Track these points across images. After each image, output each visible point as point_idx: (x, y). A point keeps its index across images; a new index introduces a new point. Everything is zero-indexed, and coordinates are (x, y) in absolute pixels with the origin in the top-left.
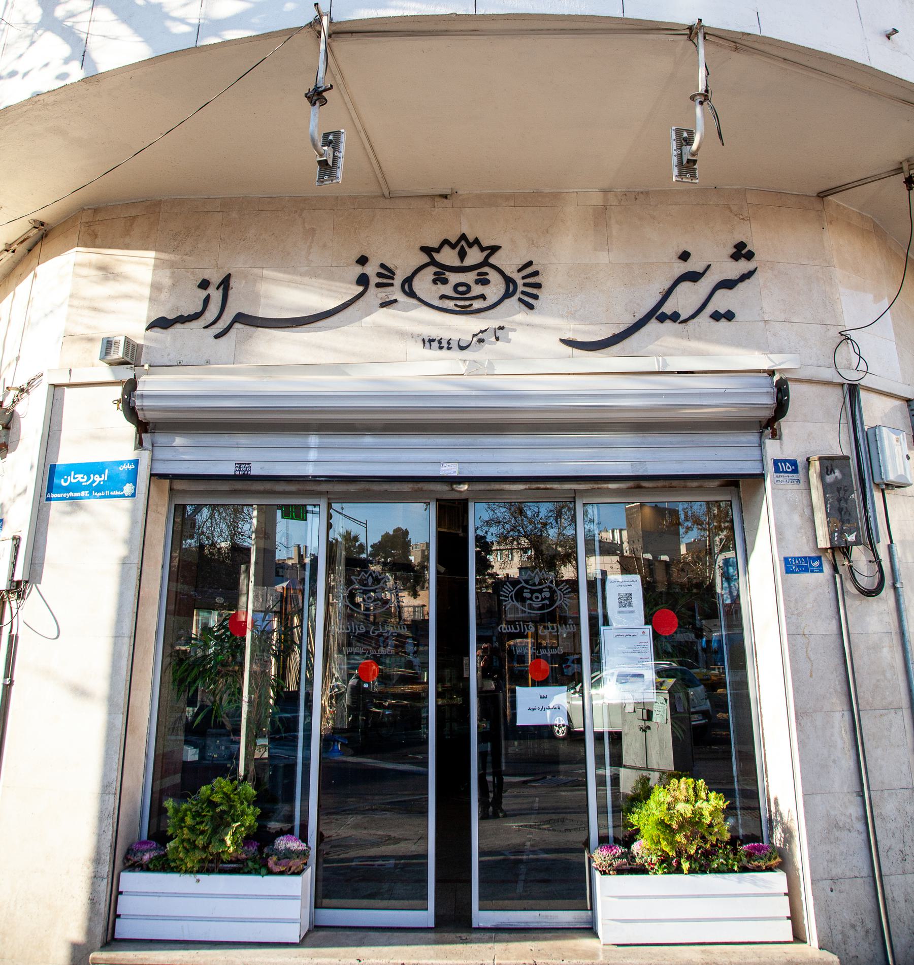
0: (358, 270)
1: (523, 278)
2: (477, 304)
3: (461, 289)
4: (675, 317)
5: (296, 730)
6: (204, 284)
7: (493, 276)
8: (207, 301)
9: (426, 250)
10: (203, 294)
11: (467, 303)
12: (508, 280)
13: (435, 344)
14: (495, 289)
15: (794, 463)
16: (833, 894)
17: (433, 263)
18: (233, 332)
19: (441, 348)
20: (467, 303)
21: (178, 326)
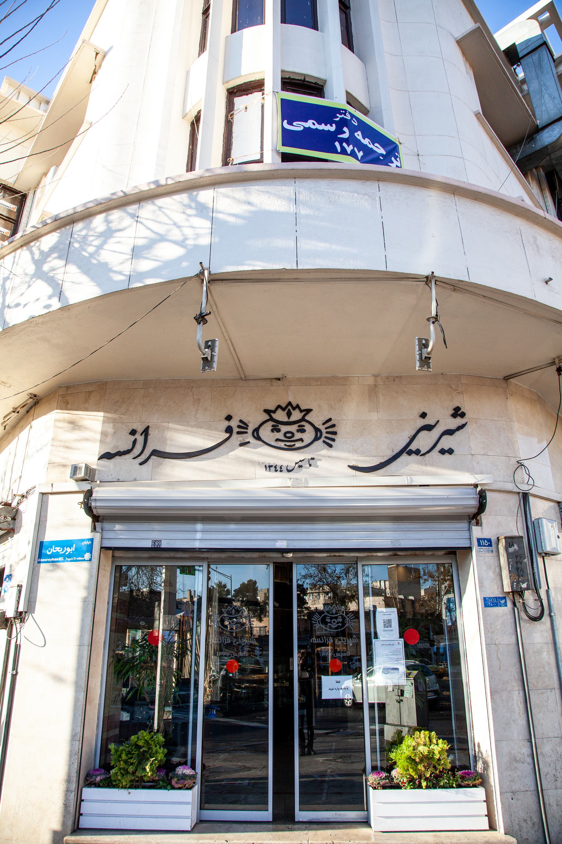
0: (226, 424)
1: (326, 428)
2: (298, 444)
3: (288, 435)
4: (417, 452)
7: (308, 427)
8: (135, 442)
9: (267, 411)
10: (132, 438)
11: (292, 444)
12: (317, 430)
13: (273, 469)
15: (489, 540)
16: (513, 801)
17: (272, 419)
18: (150, 461)
19: (276, 471)
20: (292, 444)
21: (117, 457)
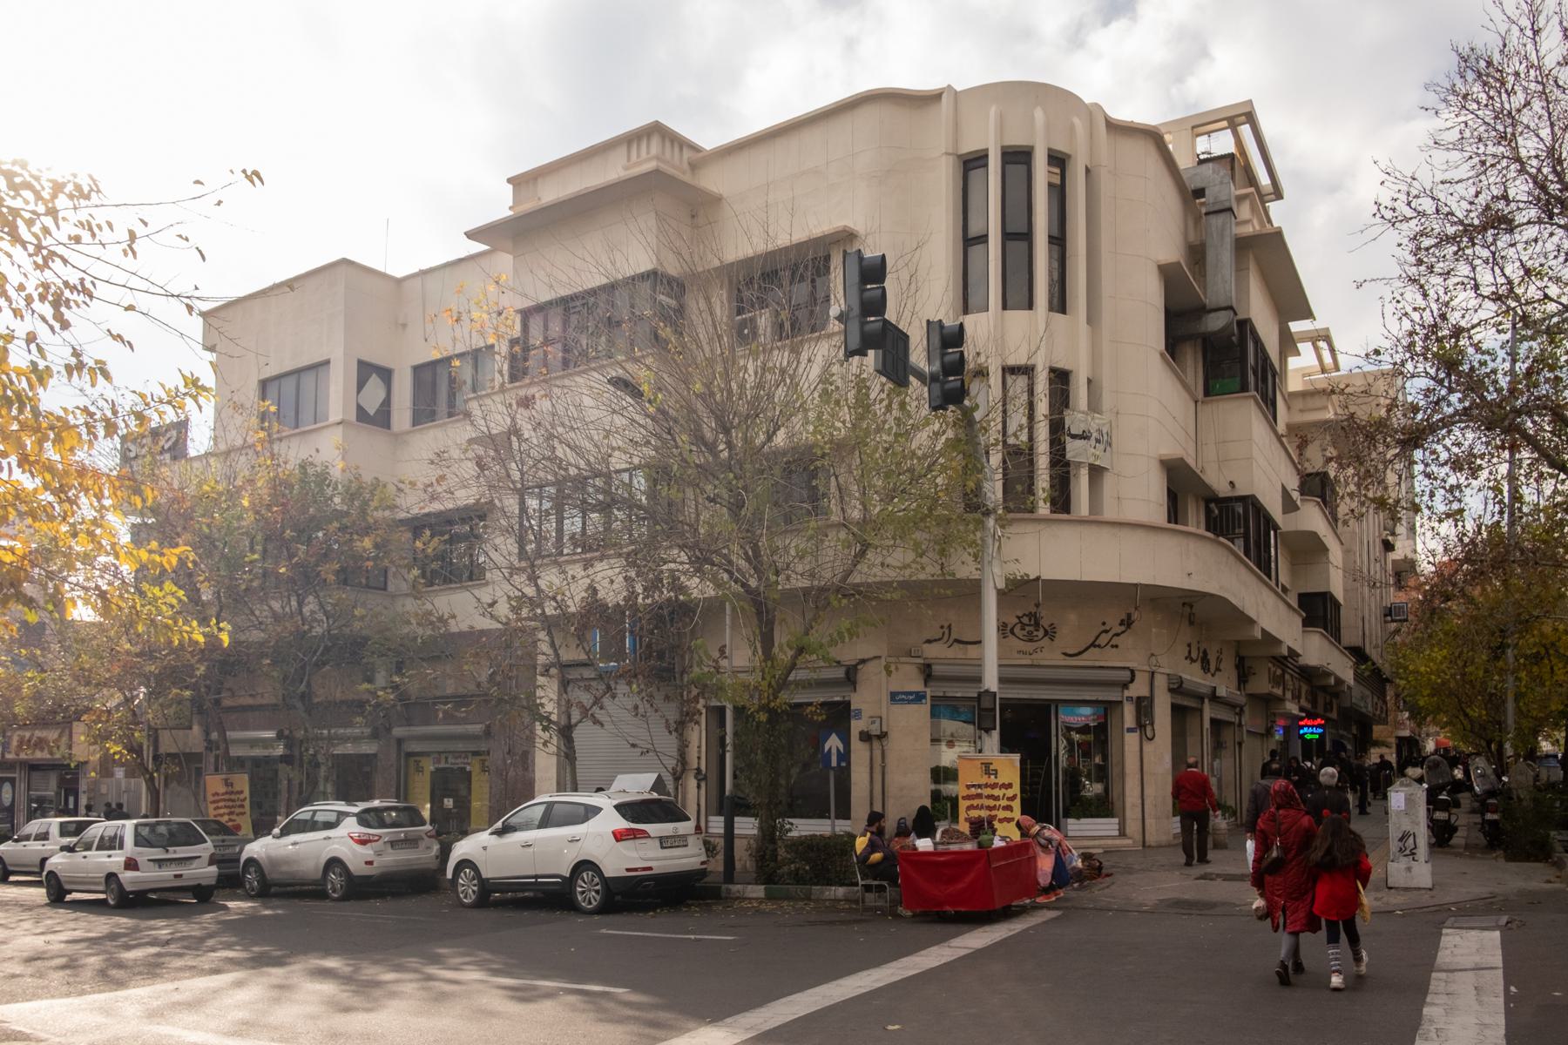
4: (1099, 646)
5: (735, 746)
6: (942, 627)
9: (1018, 617)
14: (1041, 633)
